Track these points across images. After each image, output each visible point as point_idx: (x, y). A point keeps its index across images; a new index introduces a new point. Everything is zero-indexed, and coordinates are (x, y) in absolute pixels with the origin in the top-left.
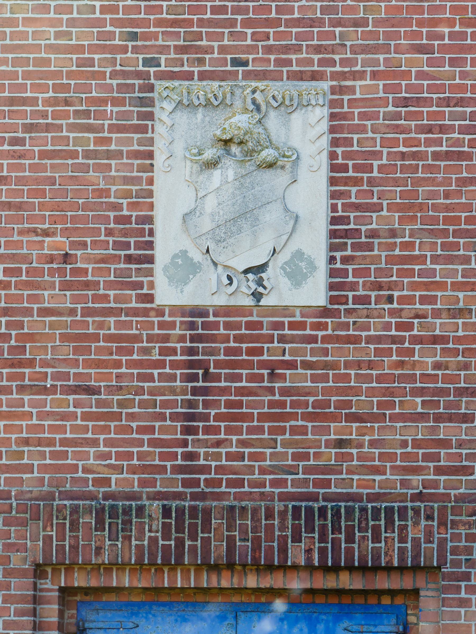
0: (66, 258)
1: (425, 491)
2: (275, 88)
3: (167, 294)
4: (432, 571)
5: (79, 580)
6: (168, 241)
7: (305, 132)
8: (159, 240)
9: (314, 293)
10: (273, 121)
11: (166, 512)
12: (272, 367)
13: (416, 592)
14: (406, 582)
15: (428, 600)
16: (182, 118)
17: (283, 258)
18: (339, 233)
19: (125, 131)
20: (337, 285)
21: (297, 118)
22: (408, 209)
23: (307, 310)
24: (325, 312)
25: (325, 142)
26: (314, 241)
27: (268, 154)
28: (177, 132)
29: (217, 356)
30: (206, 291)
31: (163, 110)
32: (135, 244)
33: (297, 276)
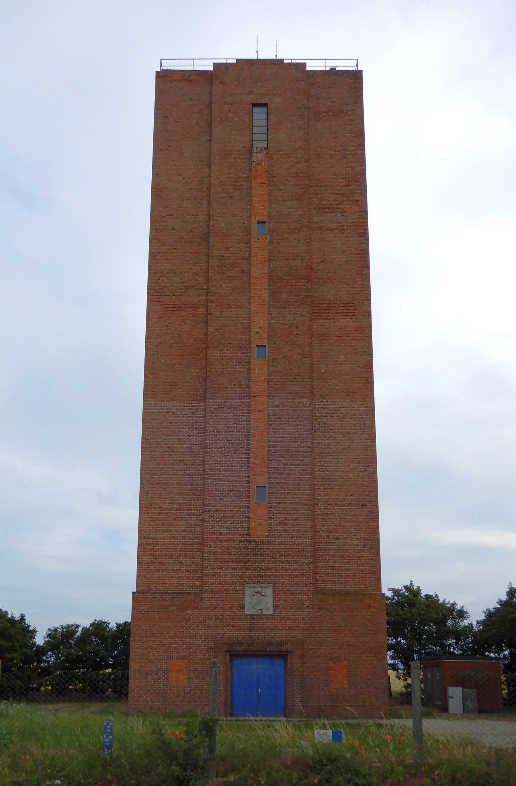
0: (231, 608)
1: (235, 735)
2: (264, 585)
3: (247, 613)
4: (290, 652)
5: (232, 653)
6: (247, 606)
7: (269, 591)
8: (246, 605)
9: (271, 612)
10: (264, 589)
11: (247, 643)
12: (264, 623)
13: (287, 655)
14: (286, 653)
15: (289, 655)
16: (249, 589)
17: (266, 608)
18: (274, 605)
19: (341, 72)
20: (274, 611)
21: (267, 589)
22: (285, 601)
23: (269, 615)
24: (272, 615)
25: (272, 592)
26: (270, 605)
27: (263, 594)
28: (248, 591)
29: (255, 621)
30: (253, 612)
31: (246, 588)
32: (242, 605)
33: (268, 610)
